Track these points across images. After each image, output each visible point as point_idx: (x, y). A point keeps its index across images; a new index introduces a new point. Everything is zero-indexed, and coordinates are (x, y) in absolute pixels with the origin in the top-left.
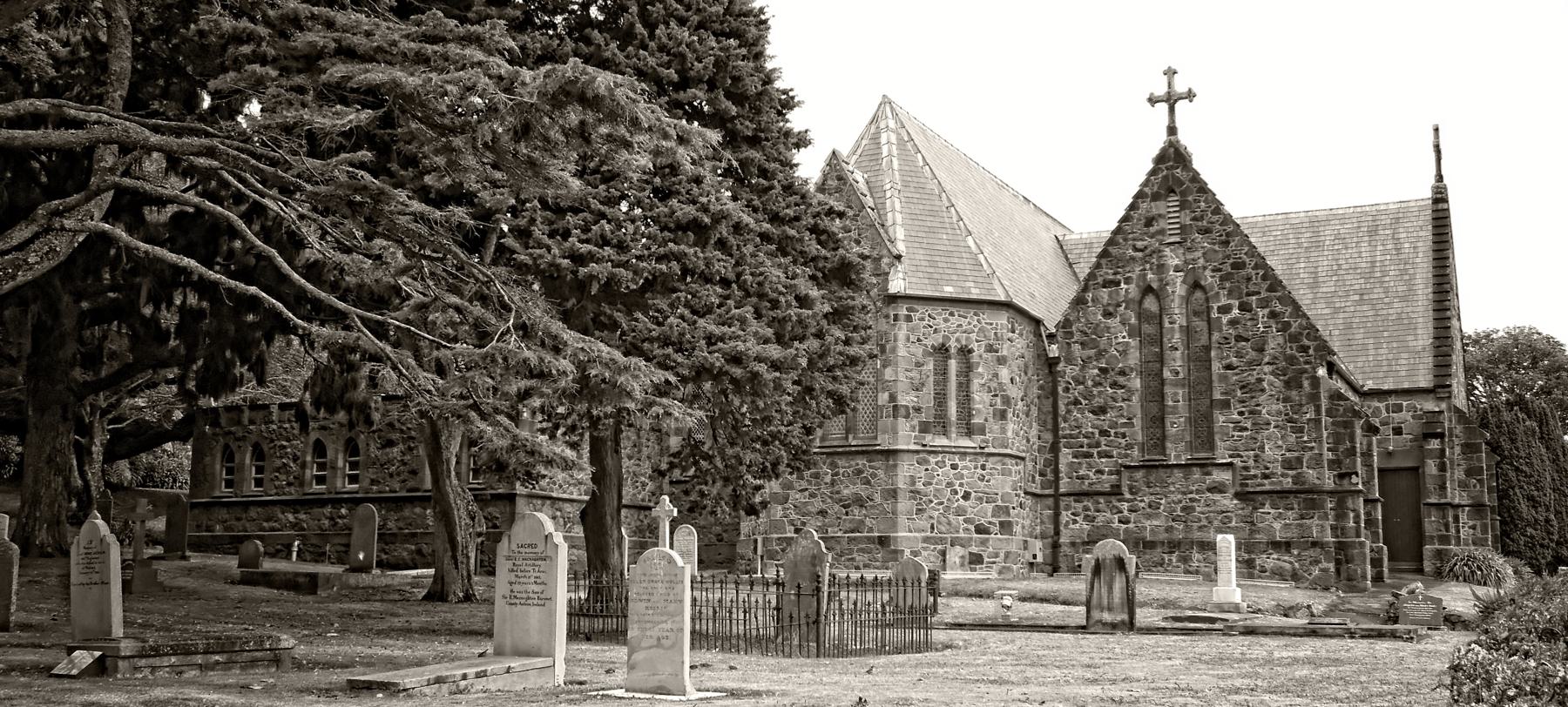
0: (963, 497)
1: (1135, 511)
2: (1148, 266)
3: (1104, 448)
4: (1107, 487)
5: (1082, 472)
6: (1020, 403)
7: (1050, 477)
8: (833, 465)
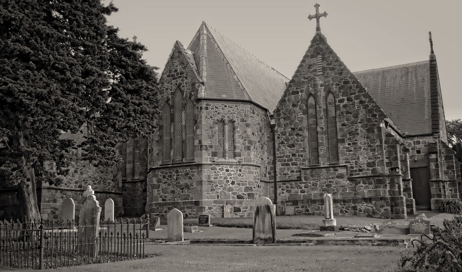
2: (310, 85)
3: (294, 161)
4: (295, 178)
5: (285, 172)
7: (273, 174)
8: (177, 172)
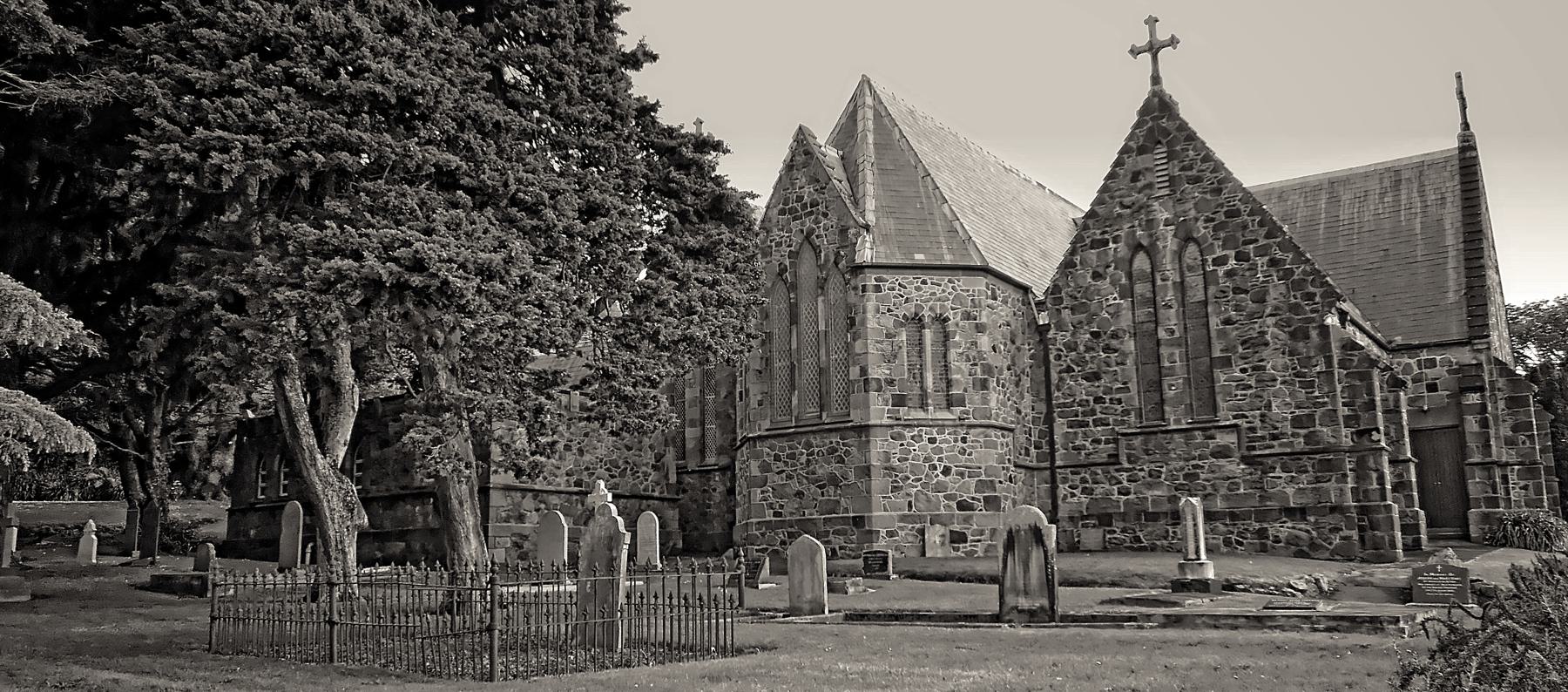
0: (943, 473)
1: (1135, 481)
3: (1099, 416)
4: (1103, 457)
6: (1006, 372)
7: (1046, 449)
